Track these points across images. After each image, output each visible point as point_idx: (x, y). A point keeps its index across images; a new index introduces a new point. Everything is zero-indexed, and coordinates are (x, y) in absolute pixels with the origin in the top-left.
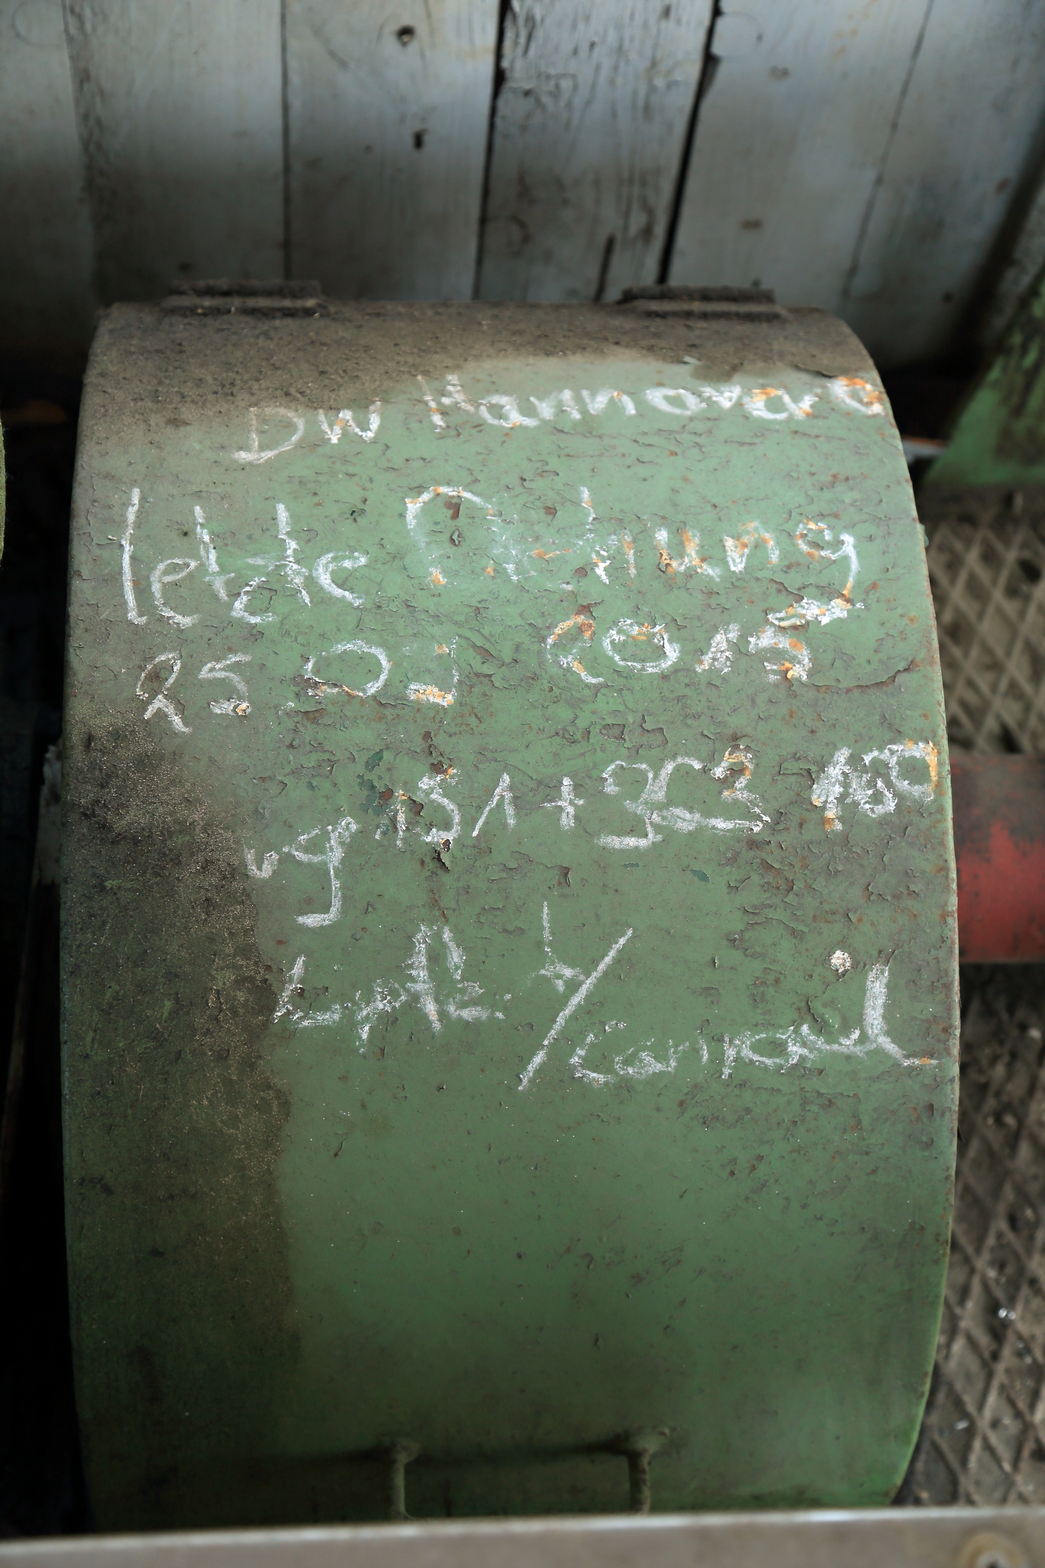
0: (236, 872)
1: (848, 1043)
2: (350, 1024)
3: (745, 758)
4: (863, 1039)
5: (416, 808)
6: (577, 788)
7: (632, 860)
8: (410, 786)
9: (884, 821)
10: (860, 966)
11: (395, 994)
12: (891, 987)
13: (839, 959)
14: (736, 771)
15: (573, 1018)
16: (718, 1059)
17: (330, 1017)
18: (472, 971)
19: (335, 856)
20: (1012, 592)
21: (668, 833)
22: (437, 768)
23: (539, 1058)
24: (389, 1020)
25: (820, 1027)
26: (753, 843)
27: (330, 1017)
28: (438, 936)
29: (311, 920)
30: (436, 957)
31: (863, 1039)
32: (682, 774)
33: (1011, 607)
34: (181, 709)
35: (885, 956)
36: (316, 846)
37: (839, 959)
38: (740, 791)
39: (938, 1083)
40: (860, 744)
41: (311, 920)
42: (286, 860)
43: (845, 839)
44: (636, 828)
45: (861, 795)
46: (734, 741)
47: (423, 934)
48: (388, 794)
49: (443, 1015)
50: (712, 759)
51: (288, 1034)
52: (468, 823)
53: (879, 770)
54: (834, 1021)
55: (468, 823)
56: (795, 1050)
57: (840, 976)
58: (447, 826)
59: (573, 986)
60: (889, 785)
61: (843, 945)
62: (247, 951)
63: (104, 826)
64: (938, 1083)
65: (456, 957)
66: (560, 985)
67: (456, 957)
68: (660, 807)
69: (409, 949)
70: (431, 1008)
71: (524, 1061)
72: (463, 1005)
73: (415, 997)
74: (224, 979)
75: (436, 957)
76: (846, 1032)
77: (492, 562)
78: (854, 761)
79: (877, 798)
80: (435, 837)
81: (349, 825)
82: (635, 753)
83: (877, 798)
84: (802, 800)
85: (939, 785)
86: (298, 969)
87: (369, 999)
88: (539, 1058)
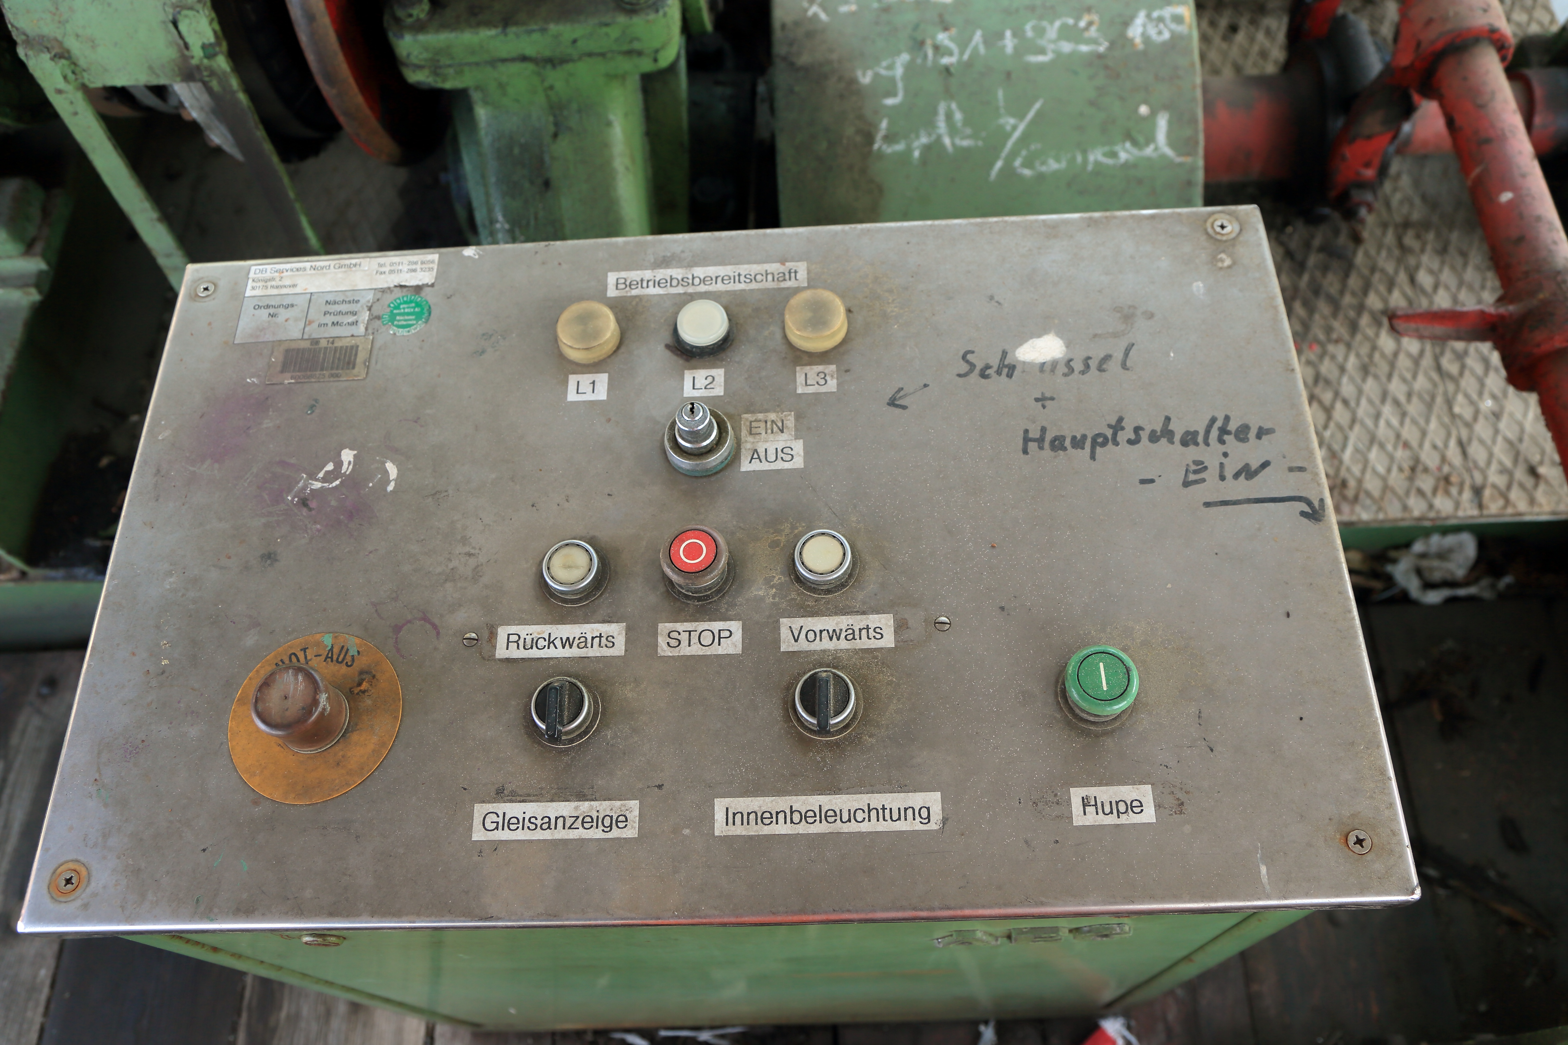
0: (853, 81)
1: (1149, 151)
2: (909, 150)
3: (1095, 17)
4: (1156, 149)
5: (937, 48)
6: (1014, 35)
7: (1041, 67)
8: (933, 38)
9: (1164, 44)
10: (1153, 113)
11: (930, 135)
12: (1170, 123)
13: (1144, 110)
14: (1090, 24)
15: (1016, 144)
16: (1085, 161)
17: (900, 147)
18: (967, 122)
19: (899, 71)
20: (1225, 38)
21: (1058, 54)
22: (946, 29)
23: (999, 164)
24: (927, 149)
25: (1135, 143)
26: (1100, 56)
27: (900, 147)
28: (949, 107)
29: (890, 102)
30: (949, 116)
31: (1156, 149)
32: (1064, 27)
33: (1224, 46)
34: (825, 9)
35: (1166, 107)
36: (890, 67)
37: (1144, 110)
38: (1093, 32)
39: (1192, 169)
40: (1150, 9)
41: (890, 102)
42: (877, 75)
43: (1145, 53)
44: (1042, 51)
45: (1152, 32)
46: (1089, 10)
47: (942, 108)
48: (922, 43)
49: (953, 144)
50: (1078, 18)
51: (880, 155)
52: (962, 53)
53: (1161, 19)
54: (1141, 139)
55: (962, 53)
56: (1123, 156)
57: (1144, 119)
58: (951, 54)
59: (1015, 128)
60: (1166, 26)
61: (1146, 102)
62: (861, 117)
63: (792, 64)
64: (1192, 169)
65: (958, 116)
66: (1008, 128)
67: (958, 116)
68: (1054, 41)
69: (935, 113)
70: (947, 141)
71: (991, 165)
72: (963, 138)
73: (939, 138)
74: (850, 131)
75: (949, 116)
76: (1147, 143)
77: (951, 946)
78: (1149, 16)
79: (1160, 33)
80: (946, 61)
81: (905, 57)
82: (1041, 18)
83: (1160, 33)
84: (1123, 35)
85: (1190, 27)
86: (884, 124)
87: (918, 137)
88: (999, 164)
